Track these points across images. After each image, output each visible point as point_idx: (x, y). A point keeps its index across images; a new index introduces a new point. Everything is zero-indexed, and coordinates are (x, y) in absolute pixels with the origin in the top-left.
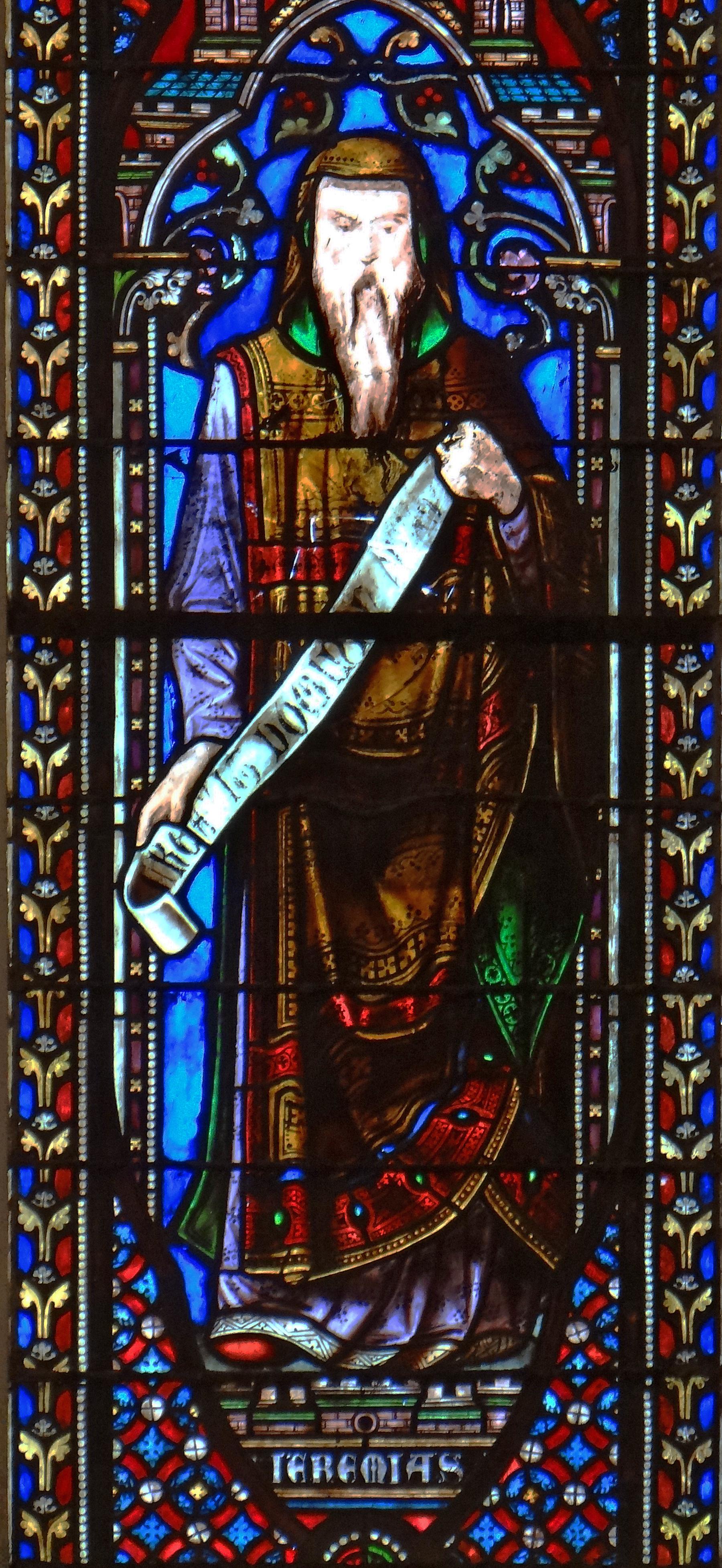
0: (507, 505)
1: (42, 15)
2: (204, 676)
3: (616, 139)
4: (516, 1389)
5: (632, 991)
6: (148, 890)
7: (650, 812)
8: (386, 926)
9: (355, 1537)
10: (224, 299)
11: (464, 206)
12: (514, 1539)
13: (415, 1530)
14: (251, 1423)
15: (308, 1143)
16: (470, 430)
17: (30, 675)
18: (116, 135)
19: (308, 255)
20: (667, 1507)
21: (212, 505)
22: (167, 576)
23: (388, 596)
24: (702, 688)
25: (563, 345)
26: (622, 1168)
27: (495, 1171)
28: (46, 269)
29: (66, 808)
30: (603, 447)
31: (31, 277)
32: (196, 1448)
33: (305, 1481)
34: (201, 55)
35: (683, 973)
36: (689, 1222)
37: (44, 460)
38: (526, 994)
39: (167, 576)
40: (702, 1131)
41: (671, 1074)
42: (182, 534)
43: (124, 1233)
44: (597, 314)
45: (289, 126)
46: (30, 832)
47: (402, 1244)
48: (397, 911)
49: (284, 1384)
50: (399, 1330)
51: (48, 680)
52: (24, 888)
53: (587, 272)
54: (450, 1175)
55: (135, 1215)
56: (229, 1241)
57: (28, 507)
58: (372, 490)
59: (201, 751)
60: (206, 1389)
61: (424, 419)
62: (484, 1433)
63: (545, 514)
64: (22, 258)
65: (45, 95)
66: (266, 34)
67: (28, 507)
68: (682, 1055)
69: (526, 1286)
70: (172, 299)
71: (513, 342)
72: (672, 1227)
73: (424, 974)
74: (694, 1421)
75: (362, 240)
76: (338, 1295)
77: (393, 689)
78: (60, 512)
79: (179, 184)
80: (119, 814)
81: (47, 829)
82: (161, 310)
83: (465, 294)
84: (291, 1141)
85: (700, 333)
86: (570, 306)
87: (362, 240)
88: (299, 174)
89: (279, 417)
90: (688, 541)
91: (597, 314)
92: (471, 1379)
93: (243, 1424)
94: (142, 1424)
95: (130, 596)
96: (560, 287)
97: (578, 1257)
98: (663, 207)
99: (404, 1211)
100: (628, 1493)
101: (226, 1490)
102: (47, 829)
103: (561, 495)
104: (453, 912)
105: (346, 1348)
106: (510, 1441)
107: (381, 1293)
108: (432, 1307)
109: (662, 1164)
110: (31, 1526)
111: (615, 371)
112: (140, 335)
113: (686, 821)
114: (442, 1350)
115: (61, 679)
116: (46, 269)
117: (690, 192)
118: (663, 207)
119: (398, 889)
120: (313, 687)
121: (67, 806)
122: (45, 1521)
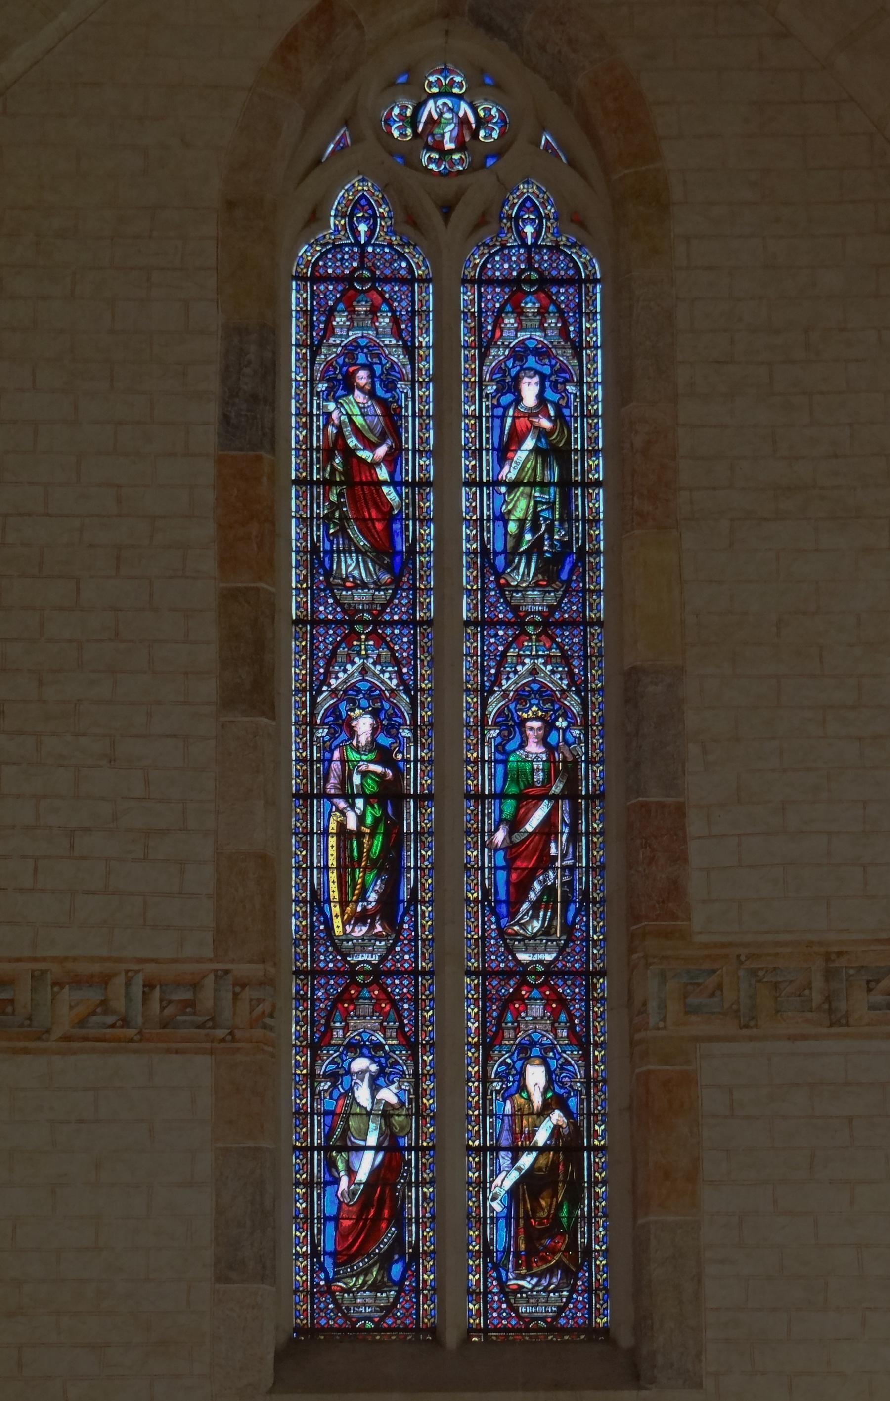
0: (564, 1126)
2: (505, 1159)
3: (586, 1057)
5: (590, 1217)
6: (494, 1199)
8: (541, 1206)
10: (508, 1088)
11: (555, 1070)
12: (568, 1323)
15: (526, 1247)
16: (557, 1112)
17: (471, 1159)
18: (487, 1057)
19: (524, 1079)
21: (506, 1126)
22: (497, 1140)
23: (541, 1144)
24: (603, 1160)
25: (575, 1095)
26: (588, 1251)
27: (563, 1252)
28: (473, 1083)
30: (583, 1115)
31: (470, 1084)
32: (504, 1306)
33: (526, 1312)
34: (504, 1042)
35: (600, 1214)
36: (602, 1262)
37: (473, 1118)
38: (569, 1218)
39: (497, 1140)
41: (598, 1233)
42: (500, 1132)
43: (490, 1265)
45: (521, 1055)
46: (471, 1189)
47: (545, 1266)
48: (543, 1203)
49: (521, 1293)
50: (544, 1283)
51: (473, 1160)
52: (470, 1199)
54: (554, 1253)
55: (492, 1261)
56: (510, 1266)
57: (470, 1127)
58: (538, 1123)
59: (504, 1174)
60: (506, 1295)
61: (548, 1110)
63: (571, 1127)
64: (469, 1080)
65: (473, 1050)
66: (516, 1038)
67: (470, 1127)
69: (570, 1275)
70: (498, 1088)
71: (565, 1095)
72: (598, 1262)
73: (548, 1215)
75: (536, 1076)
76: (532, 1276)
77: (542, 1162)
78: (476, 1128)
79: (500, 1066)
80: (488, 1185)
81: (474, 1188)
82: (496, 1090)
83: (556, 1085)
84: (523, 1247)
87: (536, 1076)
88: (523, 1064)
89: (518, 1111)
90: (600, 1132)
92: (558, 1292)
94: (493, 1301)
97: (580, 1268)
98: (595, 1070)
99: (544, 1260)
100: (590, 1314)
102: (474, 1188)
103: (575, 1124)
104: (554, 1203)
105: (534, 1286)
106: (567, 1304)
107: (541, 1275)
108: (551, 1278)
109: (596, 1251)
110: (471, 1321)
112: (492, 1094)
113: (600, 1185)
114: (552, 1286)
115: (477, 1160)
116: (473, 1083)
117: (600, 1067)
118: (595, 1070)
119: (543, 1199)
120: (526, 1160)
121: (478, 1184)
122: (474, 1320)
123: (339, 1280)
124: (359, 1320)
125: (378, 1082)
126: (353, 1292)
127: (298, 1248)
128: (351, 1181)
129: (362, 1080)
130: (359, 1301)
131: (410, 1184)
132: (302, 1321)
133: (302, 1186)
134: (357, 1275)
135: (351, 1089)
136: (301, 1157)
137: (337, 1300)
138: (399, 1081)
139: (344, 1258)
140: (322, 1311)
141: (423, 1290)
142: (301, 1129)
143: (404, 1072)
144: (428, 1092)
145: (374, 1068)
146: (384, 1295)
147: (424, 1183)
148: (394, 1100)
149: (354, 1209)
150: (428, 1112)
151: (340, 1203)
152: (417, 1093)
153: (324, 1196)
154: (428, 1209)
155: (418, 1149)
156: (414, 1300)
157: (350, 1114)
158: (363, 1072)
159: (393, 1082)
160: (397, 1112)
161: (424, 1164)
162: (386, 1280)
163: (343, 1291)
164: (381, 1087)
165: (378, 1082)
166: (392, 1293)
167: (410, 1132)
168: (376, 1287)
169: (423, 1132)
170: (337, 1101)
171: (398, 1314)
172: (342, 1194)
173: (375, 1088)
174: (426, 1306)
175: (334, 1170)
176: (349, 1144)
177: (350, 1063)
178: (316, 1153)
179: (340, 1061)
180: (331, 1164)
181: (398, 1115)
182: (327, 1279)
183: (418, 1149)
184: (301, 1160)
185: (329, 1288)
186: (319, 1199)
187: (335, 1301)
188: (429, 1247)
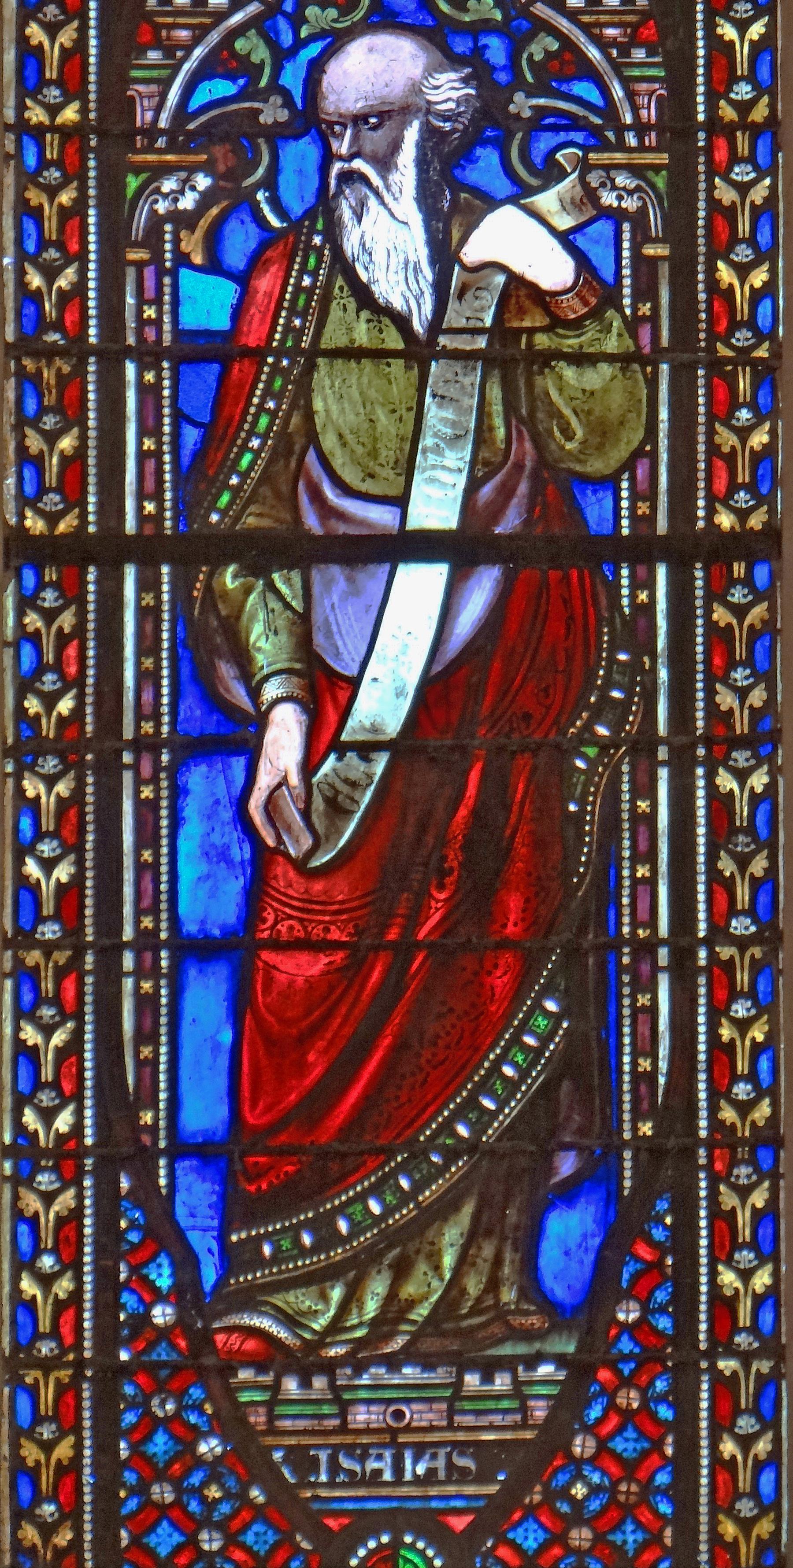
1: (51, 10)
4: (561, 1376)
7: (703, 344)
9: (385, 1539)
13: (450, 1529)
14: (271, 1418)
20: (721, 496)
29: (68, 1176)
40: (759, 418)
44: (643, 211)
53: (635, 170)
62: (524, 1425)
68: (736, 845)
74: (754, 1329)
85: (756, 1258)
86: (615, 204)
91: (643, 211)
93: (262, 1419)
95: (142, 518)
96: (603, 185)
101: (243, 1495)
111: (664, 270)
123: (249, 1299)
124: (364, 1524)
125: (473, 175)
126: (329, 1367)
127: (30, 1118)
128: (323, 737)
129: (385, 163)
130: (361, 1416)
131: (643, 746)
132: (47, 1530)
133: (50, 764)
134: (354, 1273)
135: (324, 205)
136: (49, 598)
137: (240, 1410)
138: (585, 167)
139: (275, 1159)
140: (160, 1476)
141: (711, 1355)
142: (52, 438)
143: (609, 110)
144: (744, 227)
145: (448, 90)
146: (502, 1382)
147: (722, 742)
148: (551, 268)
149: (341, 889)
150: (742, 337)
151: (262, 859)
152: (689, 232)
153: (176, 822)
154: (743, 894)
155: (685, 549)
156: (665, 1413)
157: (316, 351)
158: (385, 116)
159: (551, 173)
160: (571, 343)
161: (720, 637)
162: (508, 1295)
163: (270, 1355)
164: (492, 203)
165: (473, 175)
166: (545, 1370)
167: (645, 451)
168: (454, 1339)
169: (713, 449)
170: (243, 280)
171: (579, 1491)
172: (271, 805)
173: (450, 206)
174: (728, 1447)
175: (226, 671)
176: (311, 521)
177: (316, 68)
178: (130, 573)
179: (261, 53)
180: (206, 642)
181: (580, 359)
182: (186, 1292)
183: (685, 549)
184: (50, 616)
185: (203, 1340)
186: (147, 836)
187: (230, 1421)
188: (744, 1108)
